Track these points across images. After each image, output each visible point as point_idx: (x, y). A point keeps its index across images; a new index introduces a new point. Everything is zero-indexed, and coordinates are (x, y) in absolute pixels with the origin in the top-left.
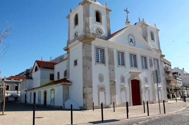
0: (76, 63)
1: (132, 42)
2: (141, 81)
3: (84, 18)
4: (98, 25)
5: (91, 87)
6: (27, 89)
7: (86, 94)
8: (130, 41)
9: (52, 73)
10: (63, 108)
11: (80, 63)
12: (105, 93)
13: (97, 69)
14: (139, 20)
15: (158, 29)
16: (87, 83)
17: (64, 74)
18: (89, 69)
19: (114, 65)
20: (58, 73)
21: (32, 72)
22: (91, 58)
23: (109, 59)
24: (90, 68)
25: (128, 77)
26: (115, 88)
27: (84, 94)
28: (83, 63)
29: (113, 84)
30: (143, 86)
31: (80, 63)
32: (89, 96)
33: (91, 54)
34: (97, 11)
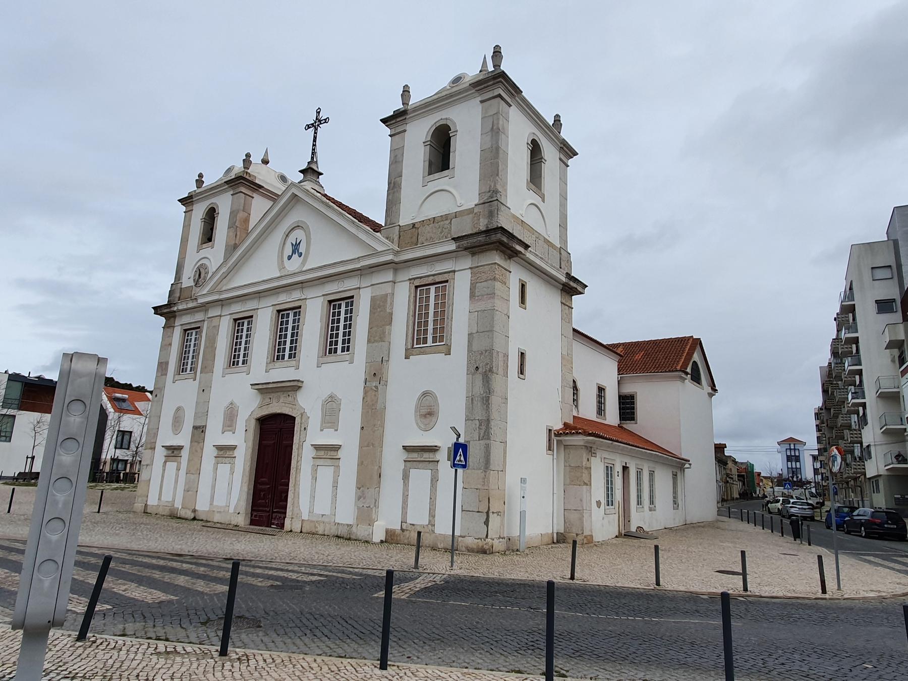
25: (250, 407)
30: (309, 437)
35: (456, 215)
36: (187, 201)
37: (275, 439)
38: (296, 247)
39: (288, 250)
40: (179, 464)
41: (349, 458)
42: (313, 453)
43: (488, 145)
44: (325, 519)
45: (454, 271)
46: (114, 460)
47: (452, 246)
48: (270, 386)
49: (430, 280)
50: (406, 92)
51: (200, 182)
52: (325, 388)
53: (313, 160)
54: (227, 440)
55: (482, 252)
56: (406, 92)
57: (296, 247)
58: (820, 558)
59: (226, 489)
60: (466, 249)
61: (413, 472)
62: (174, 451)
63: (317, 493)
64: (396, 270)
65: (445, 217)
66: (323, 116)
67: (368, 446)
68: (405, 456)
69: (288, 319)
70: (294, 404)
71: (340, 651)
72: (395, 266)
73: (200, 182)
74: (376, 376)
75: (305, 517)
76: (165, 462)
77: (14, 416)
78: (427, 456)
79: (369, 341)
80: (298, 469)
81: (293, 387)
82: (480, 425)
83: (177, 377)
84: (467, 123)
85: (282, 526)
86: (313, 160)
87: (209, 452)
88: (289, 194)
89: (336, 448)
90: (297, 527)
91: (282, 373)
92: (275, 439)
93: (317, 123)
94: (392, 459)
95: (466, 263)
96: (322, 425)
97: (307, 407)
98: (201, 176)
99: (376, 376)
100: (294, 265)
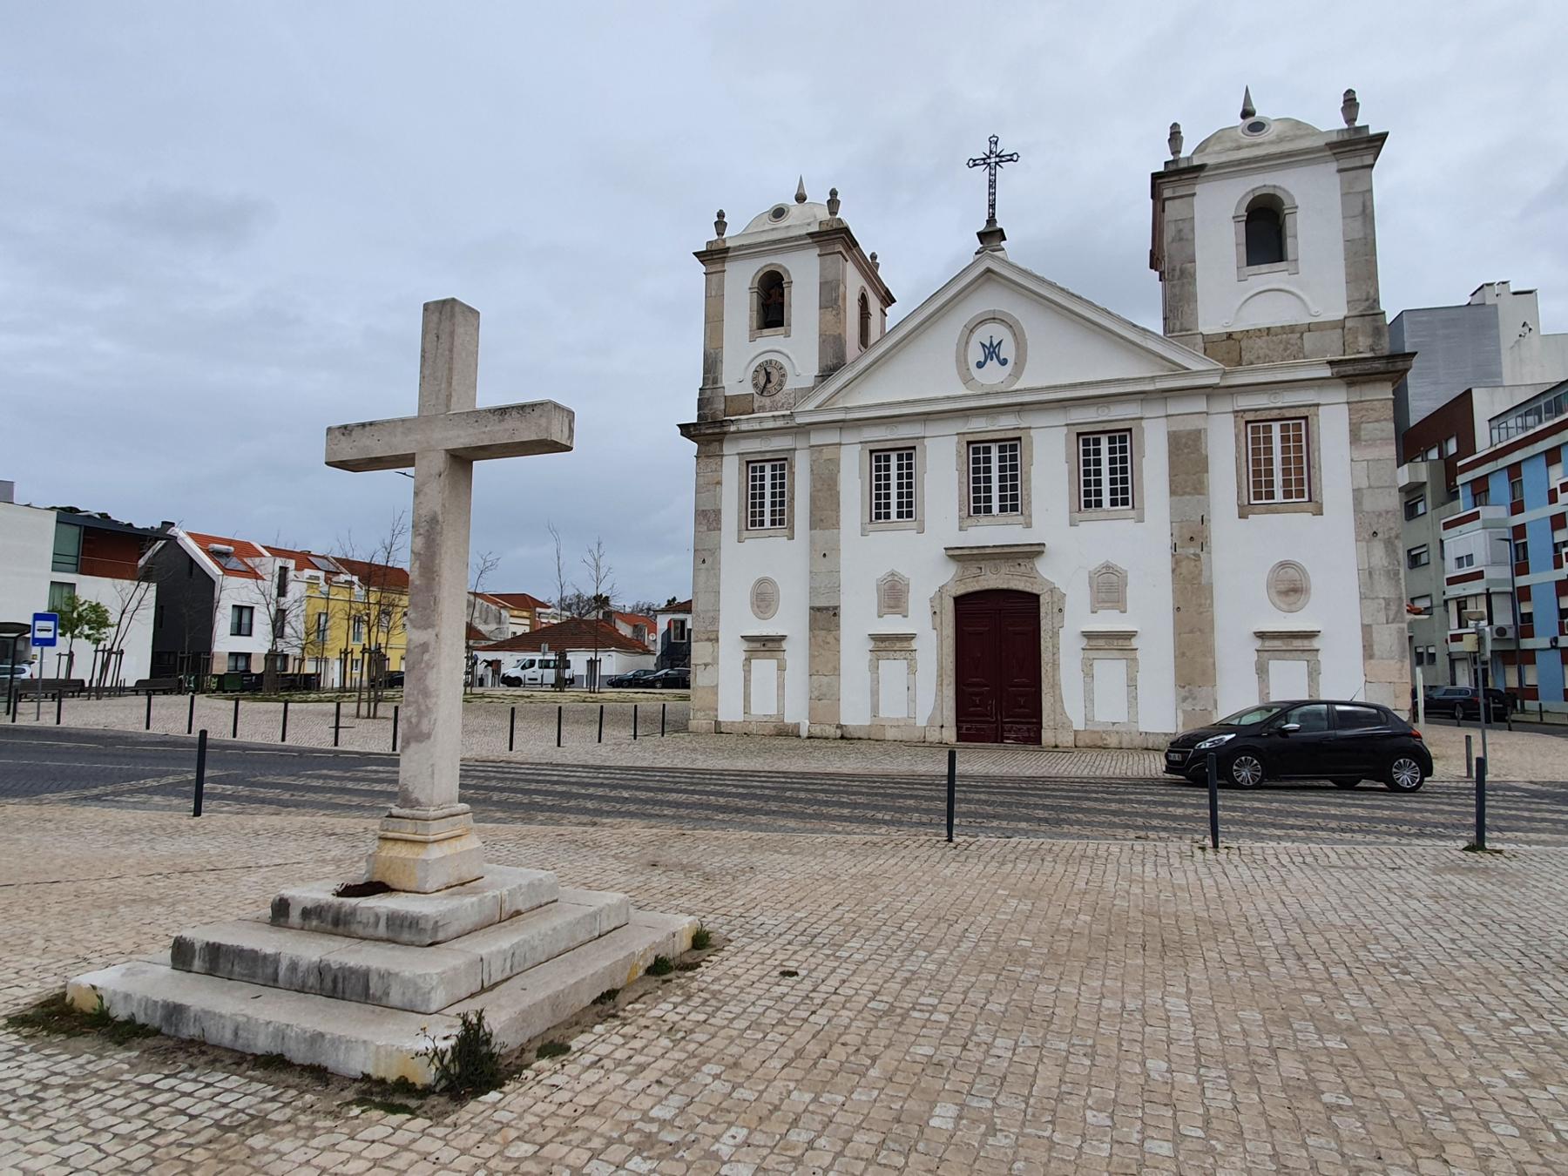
12: (781, 668)
22: (718, 513)
29: (825, 617)
35: (1309, 328)
36: (713, 256)
38: (991, 351)
39: (976, 354)
43: (1359, 235)
46: (234, 656)
47: (1327, 372)
49: (1275, 414)
50: (1175, 136)
52: (1074, 554)
53: (991, 220)
54: (893, 625)
55: (1364, 382)
56: (1175, 136)
58: (1468, 738)
61: (1275, 666)
62: (766, 645)
64: (1208, 397)
65: (1292, 329)
66: (1005, 147)
67: (1191, 632)
68: (1084, 643)
70: (1032, 576)
72: (1210, 391)
74: (1191, 543)
75: (1078, 725)
76: (748, 660)
77: (73, 585)
78: (1305, 644)
79: (1173, 492)
80: (1055, 665)
82: (1388, 604)
83: (746, 534)
85: (1037, 740)
86: (991, 220)
88: (981, 268)
90: (1067, 739)
91: (994, 532)
93: (994, 160)
95: (1340, 395)
96: (1092, 606)
98: (721, 215)
99: (1191, 543)
100: (993, 375)
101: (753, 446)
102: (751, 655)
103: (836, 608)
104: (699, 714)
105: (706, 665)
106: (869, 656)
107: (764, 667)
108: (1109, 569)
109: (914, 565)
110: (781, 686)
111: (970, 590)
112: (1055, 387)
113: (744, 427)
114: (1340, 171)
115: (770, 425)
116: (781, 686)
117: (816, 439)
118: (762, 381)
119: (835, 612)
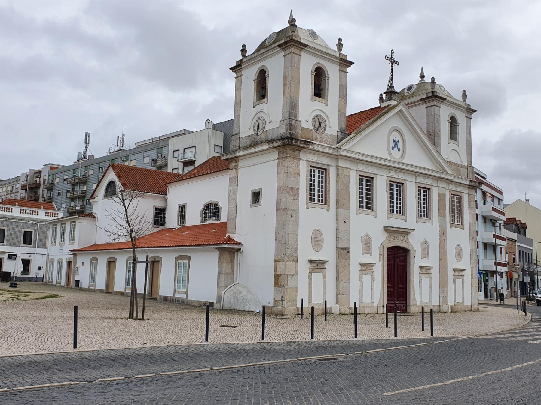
0: (256, 196)
1: (396, 149)
2: (411, 252)
3: (285, 85)
4: (318, 104)
5: (296, 261)
6: (76, 248)
7: (282, 277)
8: (392, 144)
9: (159, 204)
10: (216, 306)
11: (269, 198)
12: (324, 278)
13: (313, 219)
14: (422, 76)
15: (472, 107)
16: (285, 252)
17: (202, 214)
18: (291, 219)
19: (348, 208)
20: (182, 209)
21: (92, 197)
22: (298, 190)
23: (338, 192)
24: (294, 216)
25: (380, 241)
26: (347, 267)
27: (277, 277)
28: (278, 203)
29: (343, 252)
30: (416, 262)
31: (269, 198)
32: (290, 284)
33: (298, 182)
34: (319, 65)
37: (398, 261)
38: (396, 143)
40: (373, 276)
41: (435, 273)
42: (453, 273)
44: (428, 304)
45: (350, 169)
48: (401, 230)
51: (244, 51)
54: (367, 259)
57: (396, 143)
59: (371, 291)
60: (275, 147)
61: (457, 280)
62: (318, 265)
63: (422, 292)
66: (389, 55)
69: (397, 189)
70: (407, 242)
71: (54, 356)
73: (244, 51)
81: (406, 232)
84: (275, 65)
87: (450, 274)
89: (429, 268)
91: (396, 222)
92: (398, 261)
94: (450, 274)
97: (414, 243)
98: (244, 46)
100: (396, 155)
101: (314, 158)
102: (312, 271)
103: (349, 249)
104: (289, 304)
105: (292, 275)
106: (359, 273)
107: (317, 277)
108: (317, 231)
109: (370, 230)
110: (324, 288)
111: (392, 246)
112: (376, 157)
113: (316, 148)
114: (466, 117)
115: (326, 150)
116: (324, 288)
117: (342, 163)
118: (317, 125)
119: (347, 250)
